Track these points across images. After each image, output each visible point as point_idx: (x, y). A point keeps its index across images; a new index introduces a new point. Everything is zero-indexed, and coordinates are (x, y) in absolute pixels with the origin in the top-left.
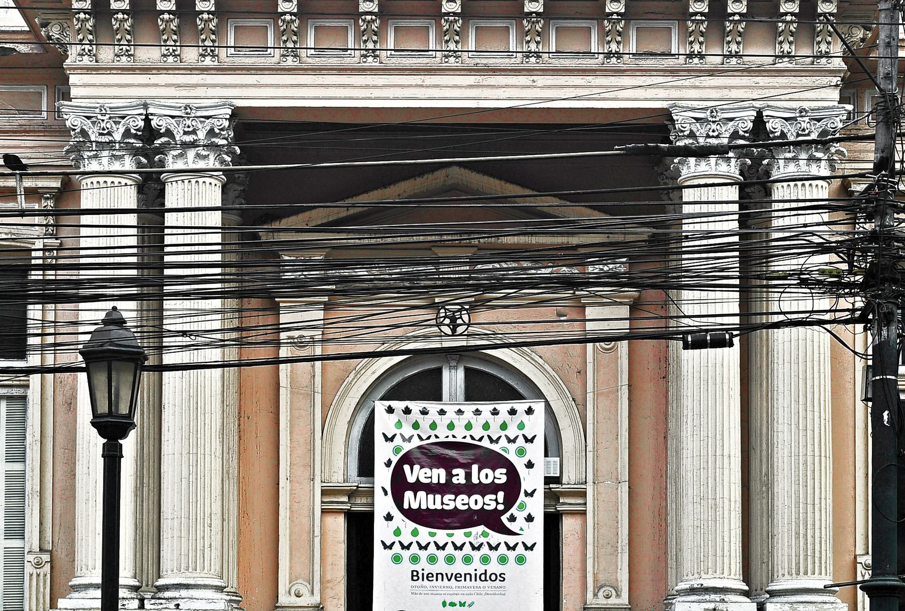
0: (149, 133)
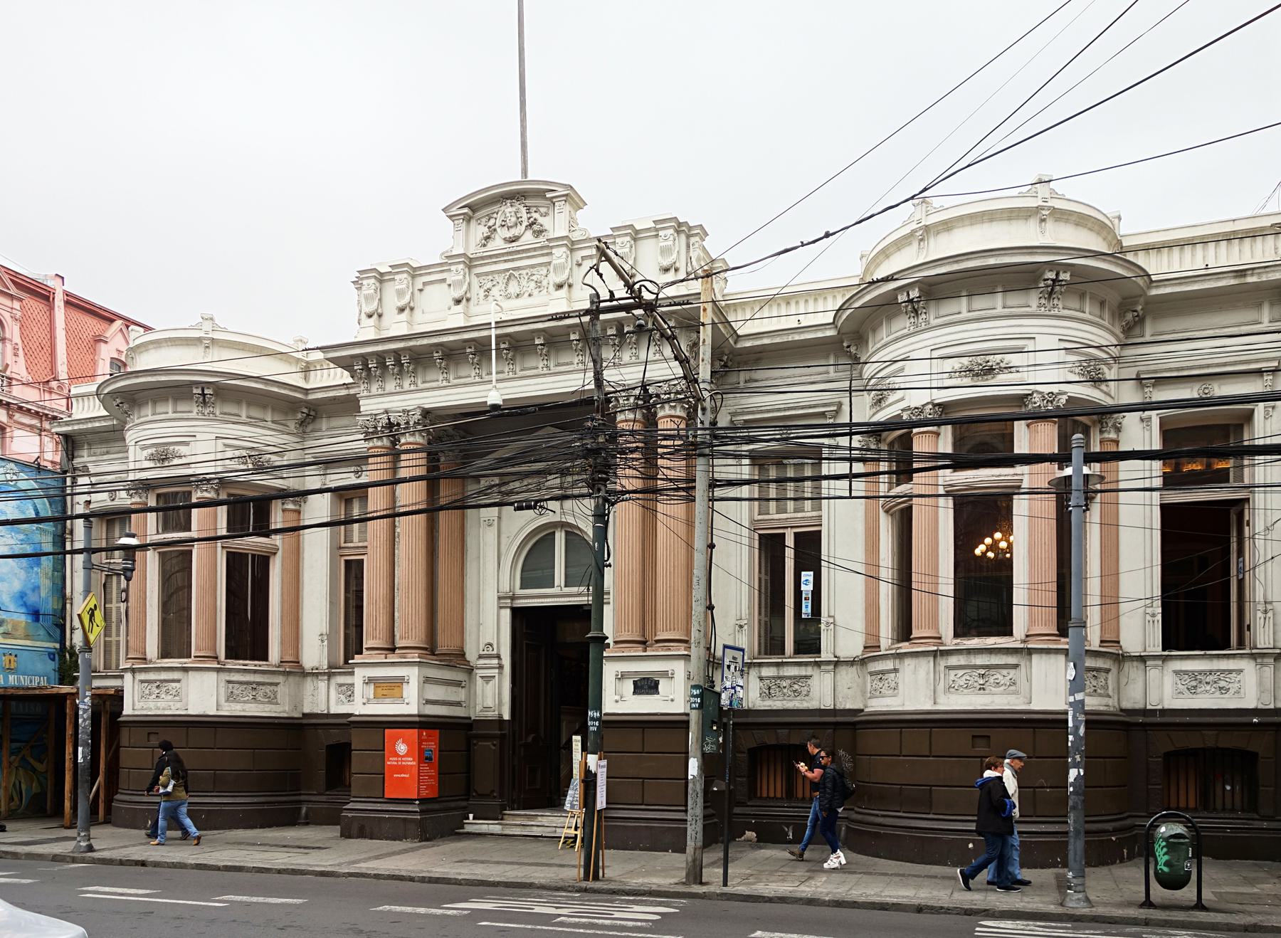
0: (390, 425)
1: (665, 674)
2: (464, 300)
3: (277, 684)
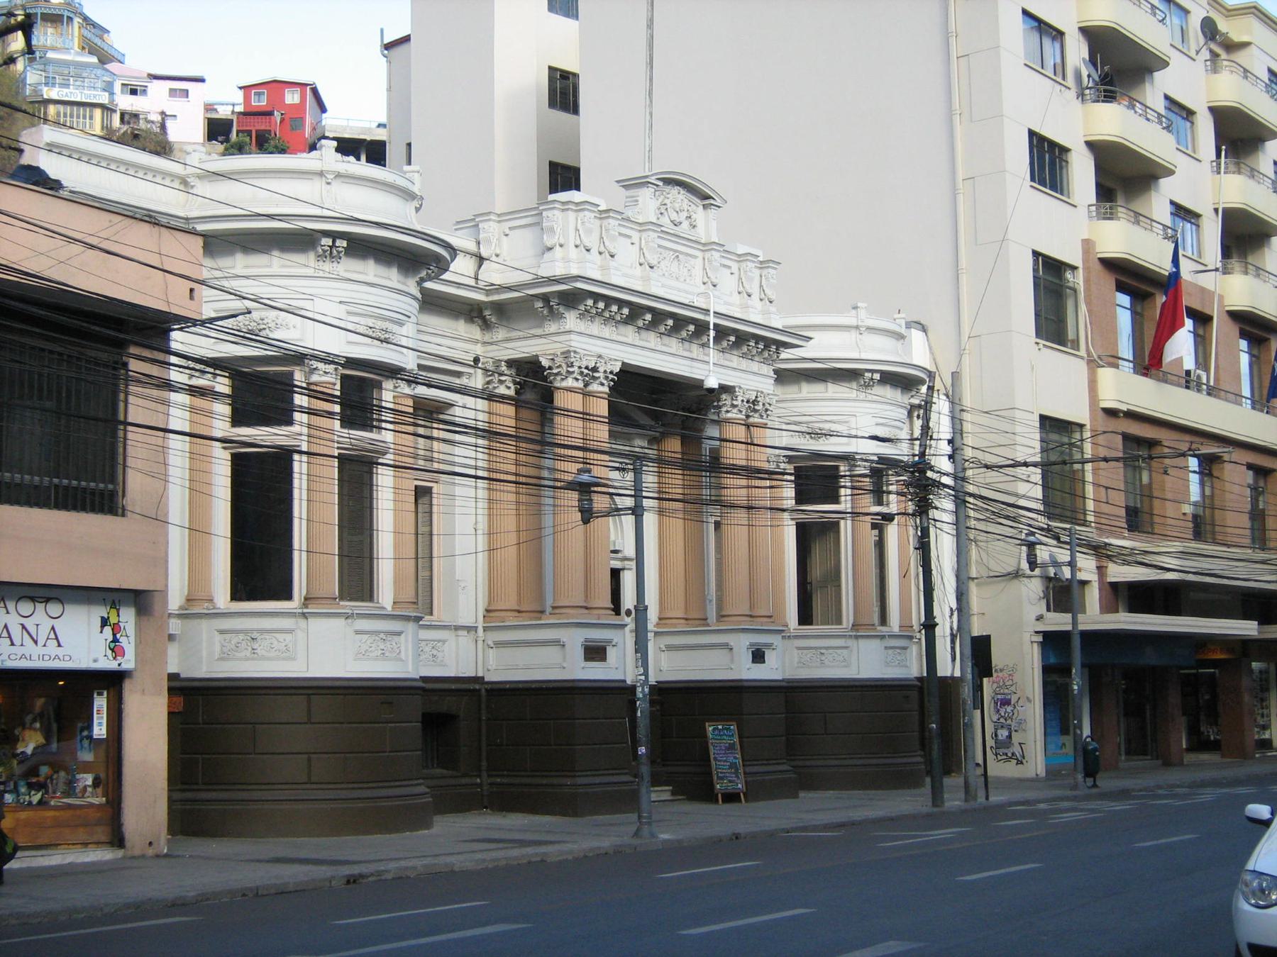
1: (769, 646)
2: (558, 246)
3: (399, 634)
